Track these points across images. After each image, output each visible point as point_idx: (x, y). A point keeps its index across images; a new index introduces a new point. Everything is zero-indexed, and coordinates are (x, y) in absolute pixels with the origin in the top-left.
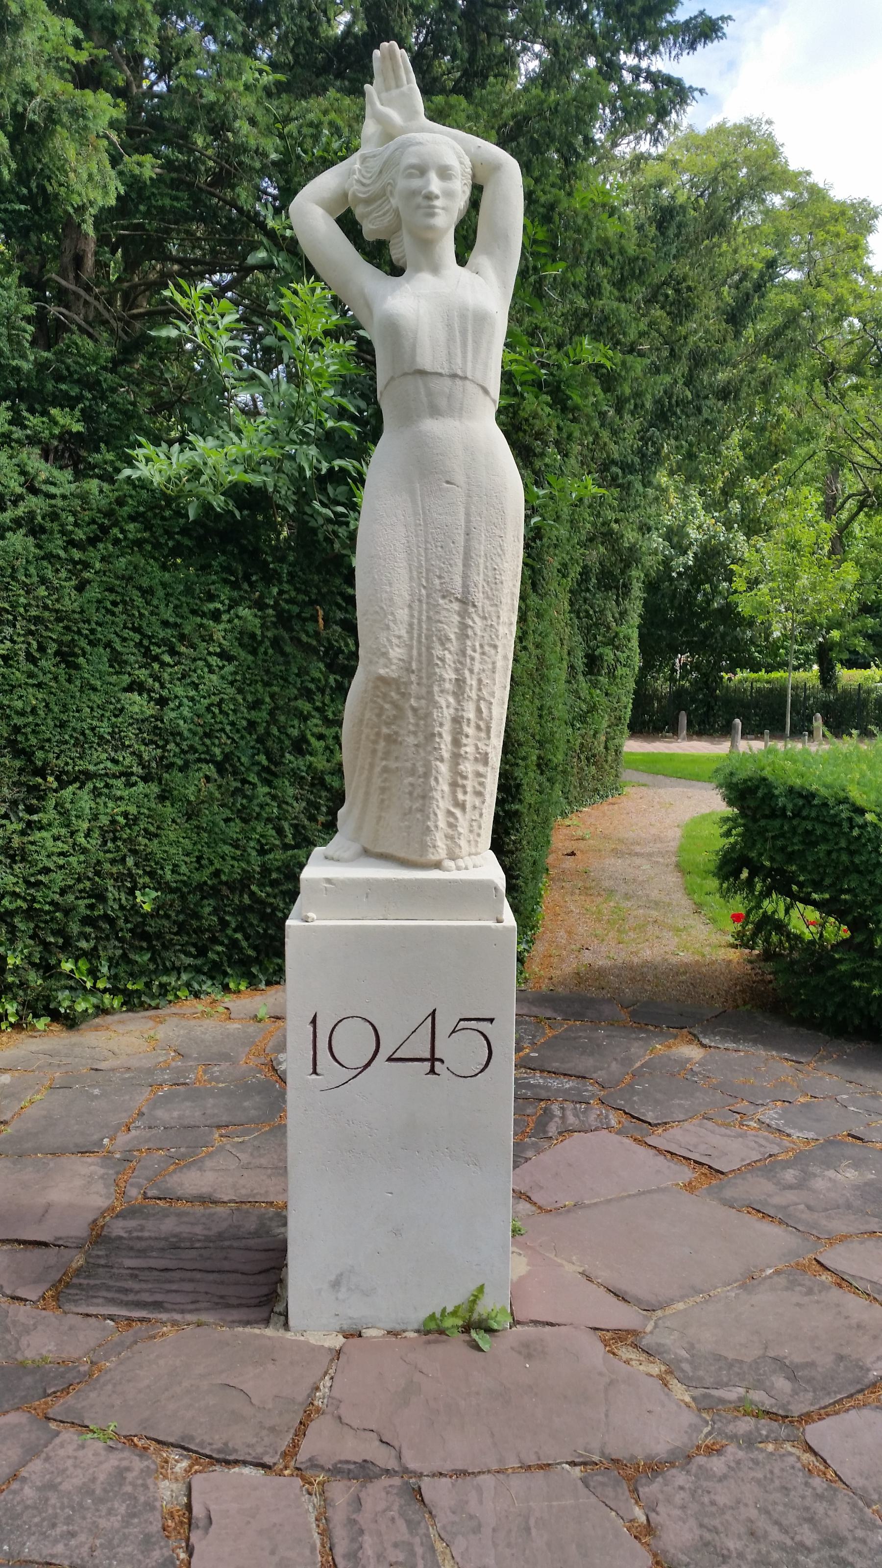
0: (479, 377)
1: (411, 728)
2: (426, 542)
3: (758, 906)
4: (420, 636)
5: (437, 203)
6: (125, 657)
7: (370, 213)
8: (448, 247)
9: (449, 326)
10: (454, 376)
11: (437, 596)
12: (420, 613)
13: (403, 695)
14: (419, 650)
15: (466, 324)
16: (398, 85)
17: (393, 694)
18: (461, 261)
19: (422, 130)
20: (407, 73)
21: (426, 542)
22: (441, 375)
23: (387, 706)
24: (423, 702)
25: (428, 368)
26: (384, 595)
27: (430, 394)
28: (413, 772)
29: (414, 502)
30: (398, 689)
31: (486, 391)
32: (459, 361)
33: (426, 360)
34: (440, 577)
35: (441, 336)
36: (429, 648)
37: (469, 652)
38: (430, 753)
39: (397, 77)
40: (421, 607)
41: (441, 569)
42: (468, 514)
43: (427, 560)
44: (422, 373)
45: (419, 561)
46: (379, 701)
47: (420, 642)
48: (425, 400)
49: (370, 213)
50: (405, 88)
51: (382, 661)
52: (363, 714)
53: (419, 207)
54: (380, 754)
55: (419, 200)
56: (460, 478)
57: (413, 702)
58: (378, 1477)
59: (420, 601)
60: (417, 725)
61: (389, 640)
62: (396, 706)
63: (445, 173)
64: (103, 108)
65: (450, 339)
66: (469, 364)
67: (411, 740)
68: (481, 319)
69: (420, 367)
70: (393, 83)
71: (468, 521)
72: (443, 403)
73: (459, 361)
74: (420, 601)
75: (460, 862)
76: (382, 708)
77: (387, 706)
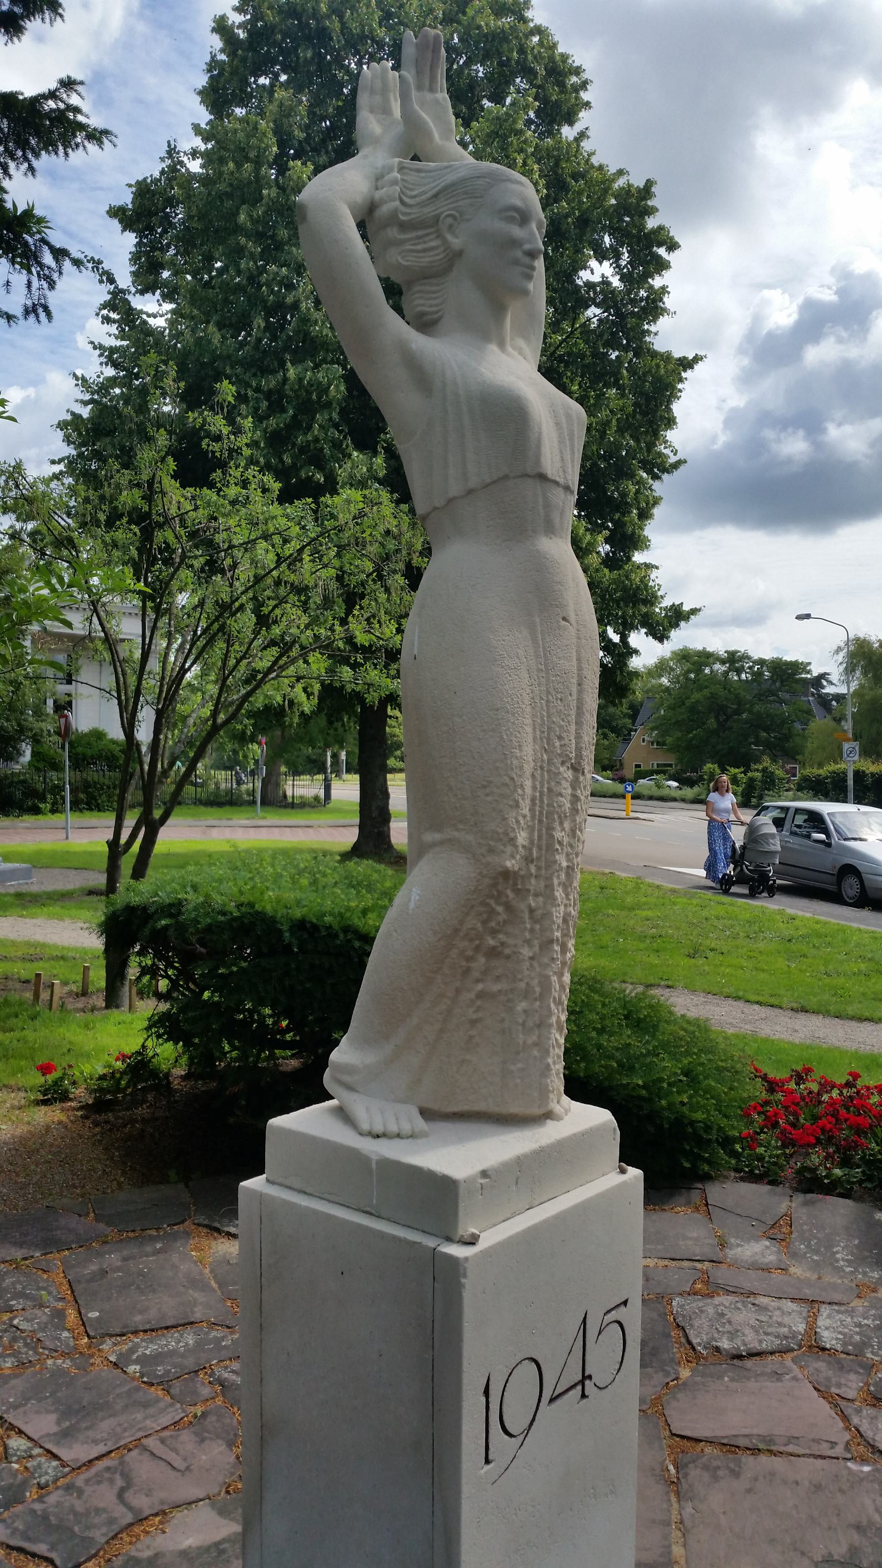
1: (527, 935)
2: (548, 692)
4: (541, 813)
7: (403, 242)
11: (557, 761)
12: (542, 786)
13: (517, 891)
14: (540, 830)
17: (509, 892)
21: (548, 692)
22: (557, 483)
23: (500, 909)
24: (541, 899)
26: (515, 762)
27: (547, 505)
28: (527, 994)
29: (534, 640)
30: (515, 884)
34: (560, 738)
36: (550, 828)
38: (547, 966)
39: (433, 79)
40: (542, 776)
41: (561, 727)
43: (549, 716)
44: (542, 477)
45: (542, 718)
46: (492, 902)
47: (540, 821)
49: (403, 242)
51: (509, 849)
52: (461, 922)
53: (516, 262)
54: (476, 974)
55: (519, 254)
56: (572, 617)
57: (532, 902)
59: (542, 768)
60: (532, 931)
61: (518, 822)
62: (508, 907)
67: (526, 952)
69: (543, 471)
70: (427, 83)
74: (542, 768)
76: (492, 912)
77: (500, 909)
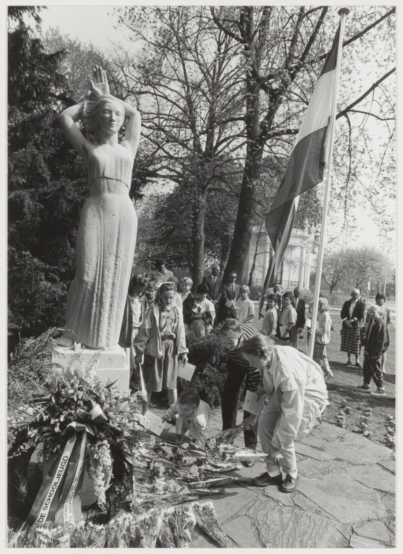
5: (113, 123)
6: (133, 536)
8: (115, 137)
9: (117, 164)
10: (117, 180)
15: (120, 162)
16: (101, 81)
19: (109, 98)
25: (109, 177)
29: (100, 220)
31: (127, 186)
32: (119, 175)
33: (107, 174)
35: (114, 166)
42: (119, 226)
44: (107, 178)
50: (103, 83)
63: (117, 114)
64: (392, 55)
66: (123, 176)
68: (127, 162)
71: (119, 229)
72: (112, 188)
75: (110, 347)
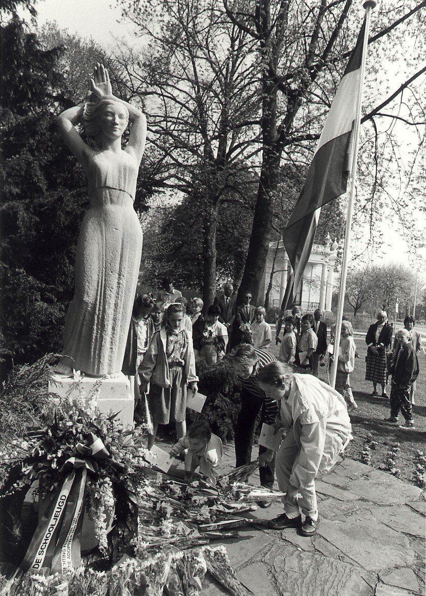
0: (130, 191)
3: (104, 506)
9: (120, 172)
10: (120, 190)
15: (124, 171)
18: (124, 146)
19: (112, 99)
20: (107, 77)
32: (123, 184)
33: (110, 183)
37: (120, 293)
44: (109, 188)
48: (109, 198)
50: (105, 83)
56: (121, 229)
58: (342, 394)
63: (121, 116)
65: (120, 177)
68: (131, 170)
72: (115, 199)
73: (123, 184)
75: (112, 375)
